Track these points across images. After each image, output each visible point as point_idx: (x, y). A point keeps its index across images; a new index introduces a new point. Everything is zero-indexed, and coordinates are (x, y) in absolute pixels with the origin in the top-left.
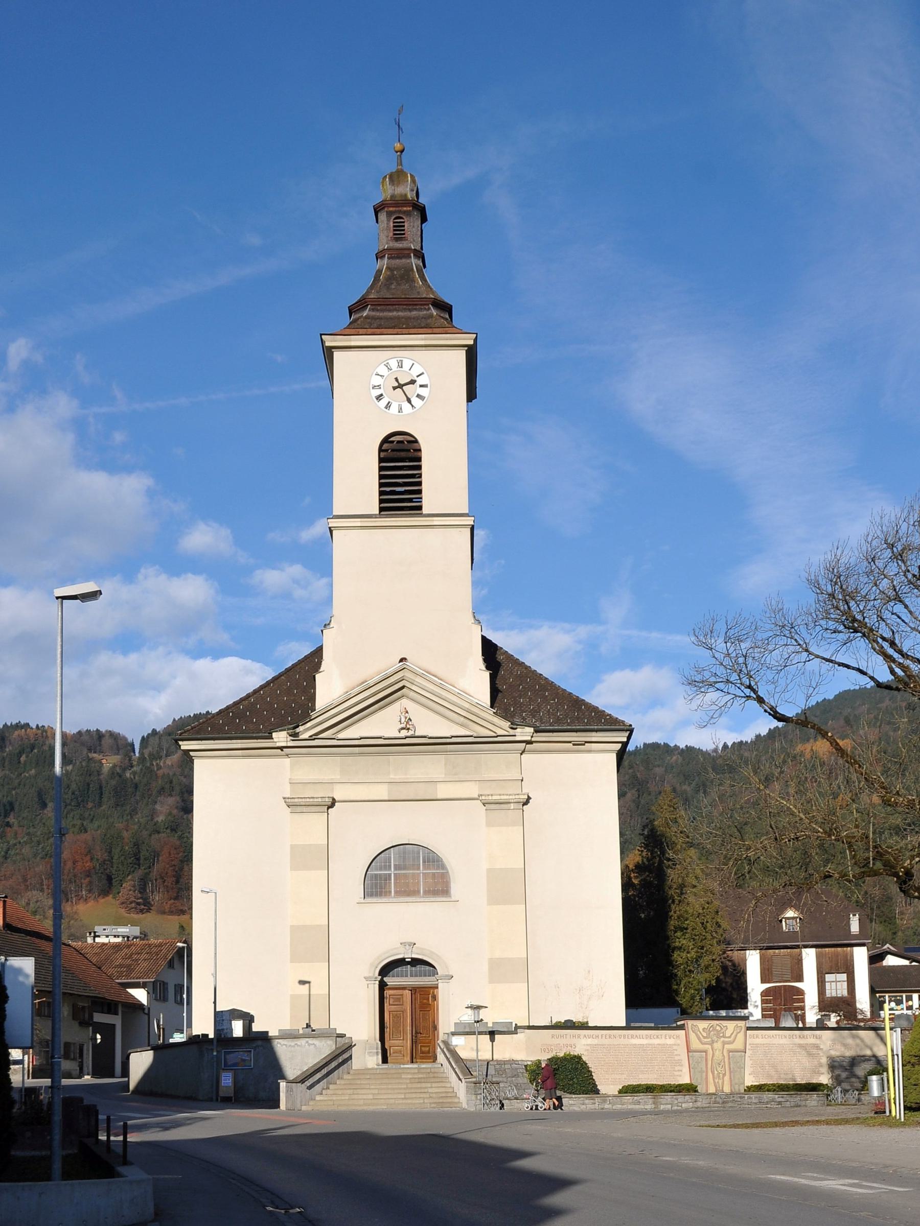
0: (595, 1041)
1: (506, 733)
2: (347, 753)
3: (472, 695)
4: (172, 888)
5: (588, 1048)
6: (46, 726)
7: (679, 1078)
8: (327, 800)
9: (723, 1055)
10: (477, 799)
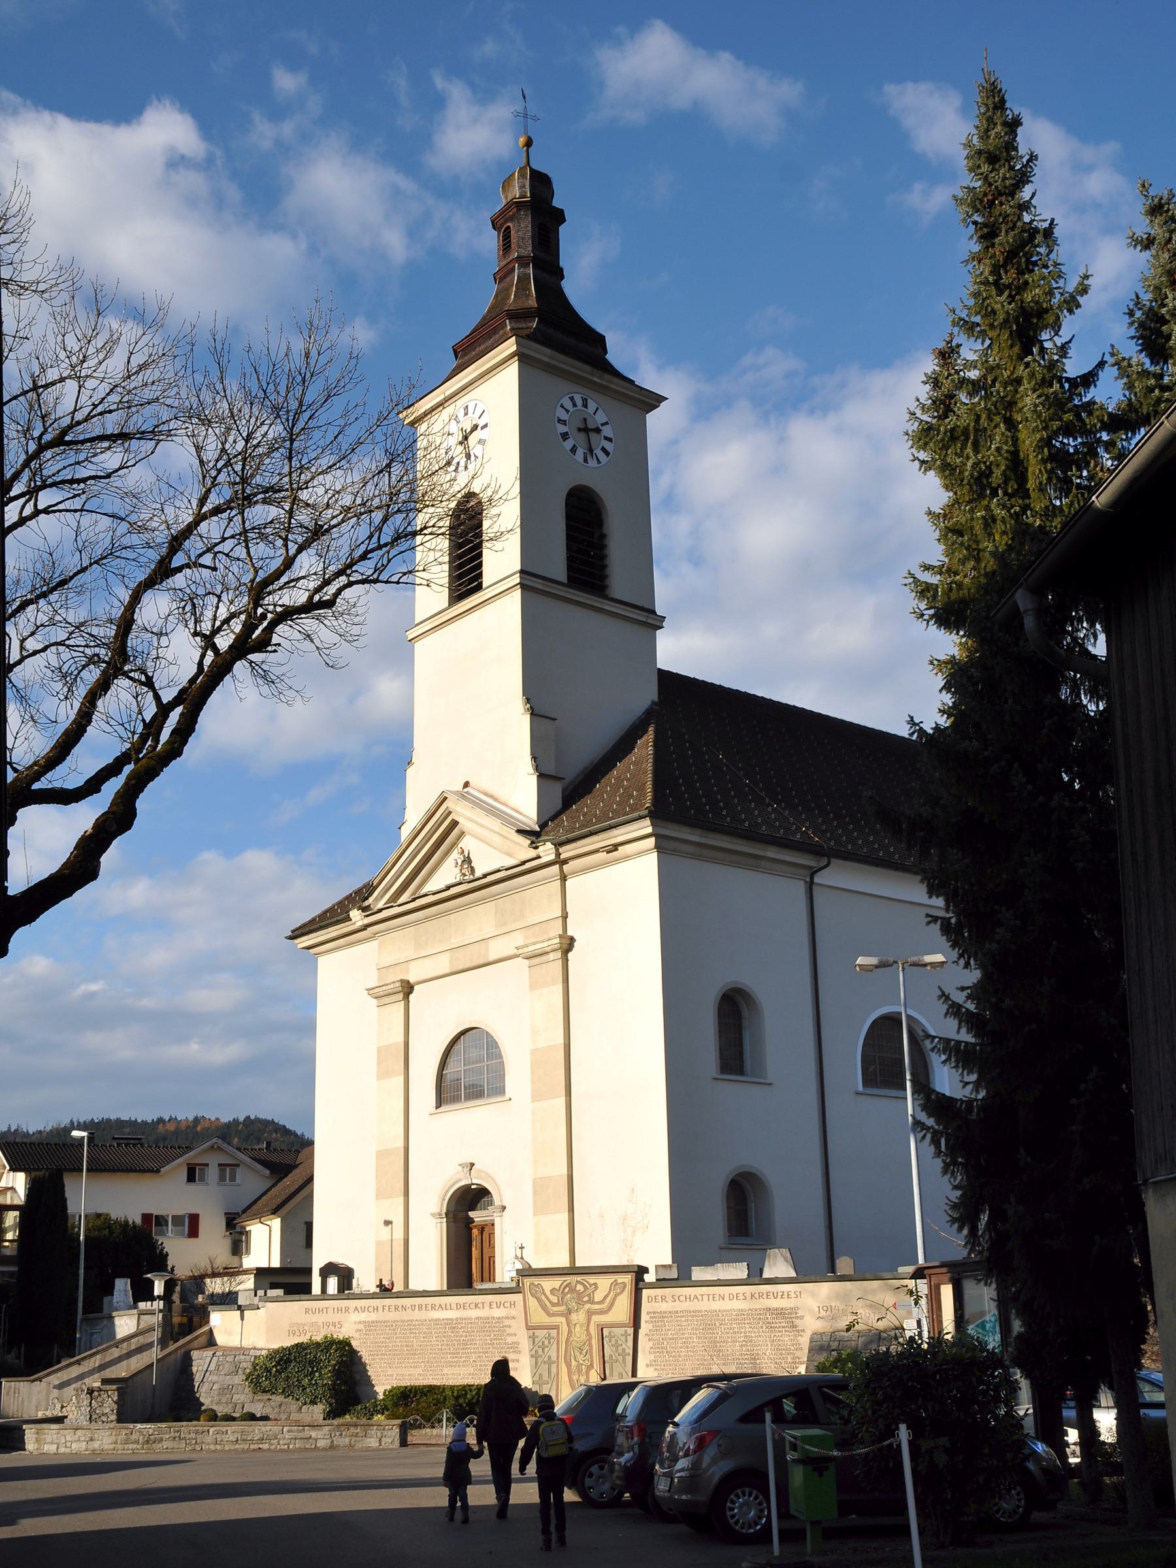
0: (373, 1317)
2: (395, 926)
5: (361, 1327)
9: (589, 1334)
10: (517, 956)
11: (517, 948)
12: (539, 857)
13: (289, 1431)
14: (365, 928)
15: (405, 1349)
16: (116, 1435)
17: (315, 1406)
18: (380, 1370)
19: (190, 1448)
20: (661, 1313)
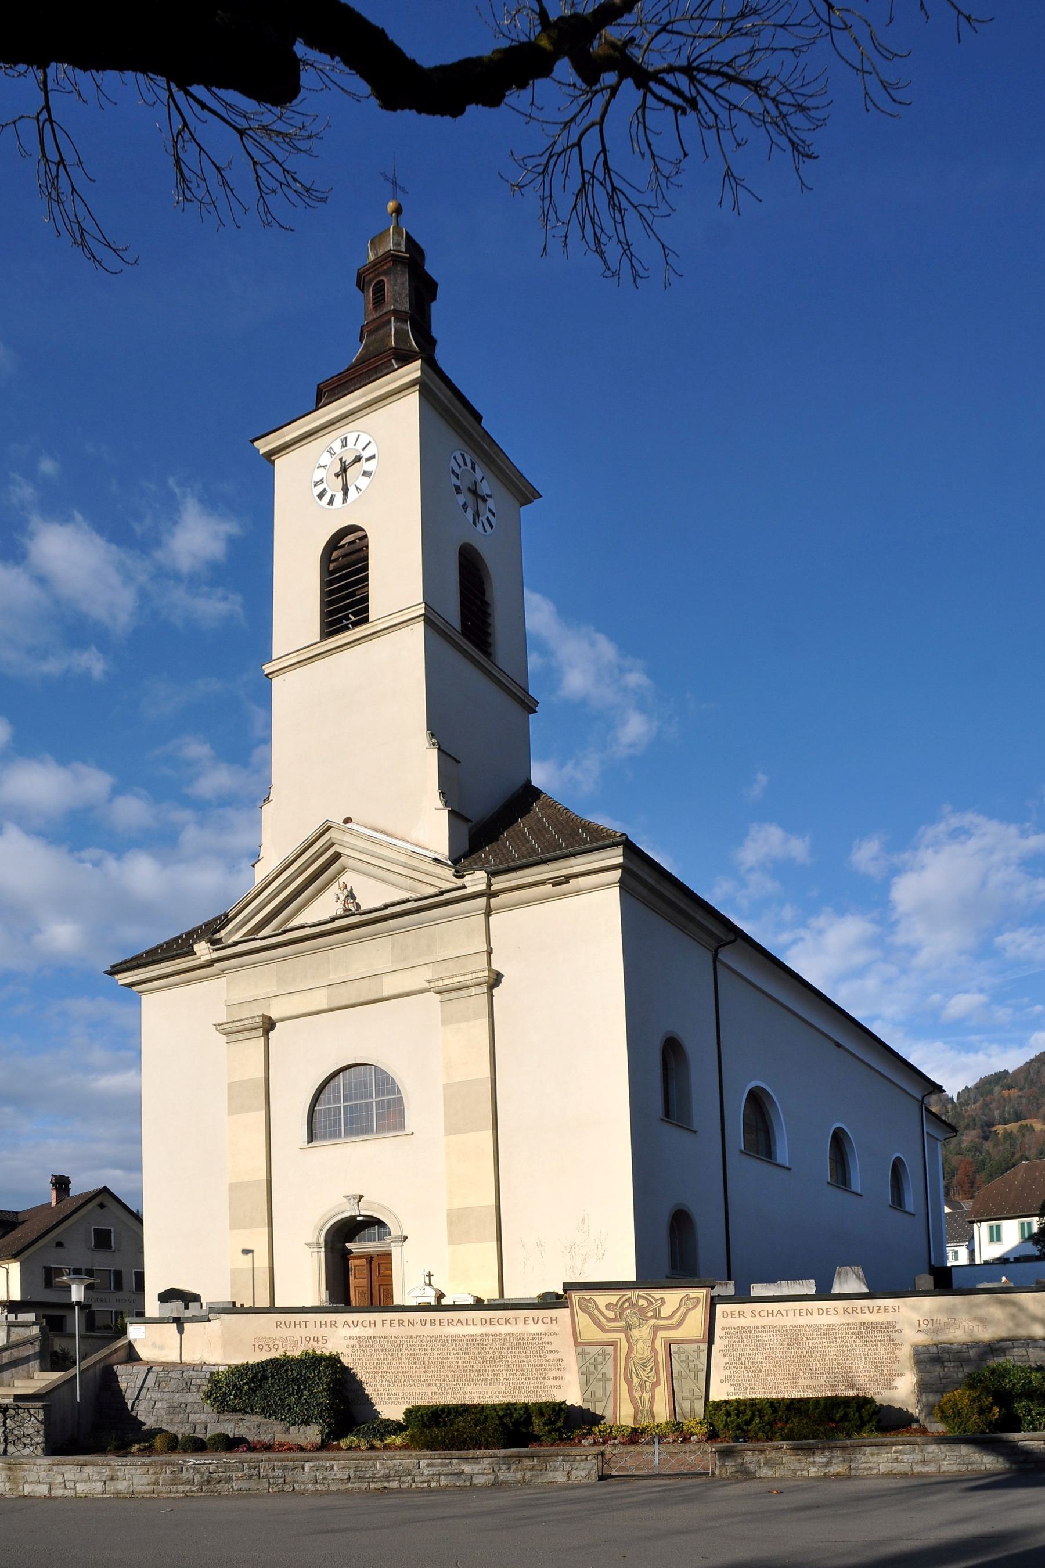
0: (370, 1332)
1: (452, 886)
2: (279, 956)
3: (426, 846)
4: (968, 1191)
5: (354, 1342)
7: (554, 1391)
8: (257, 1020)
11: (428, 982)
12: (464, 887)
13: (428, 1466)
14: (211, 963)
15: (414, 1366)
16: (156, 1473)
17: (309, 1427)
18: (381, 1389)
19: (276, 1489)
20: (738, 1328)
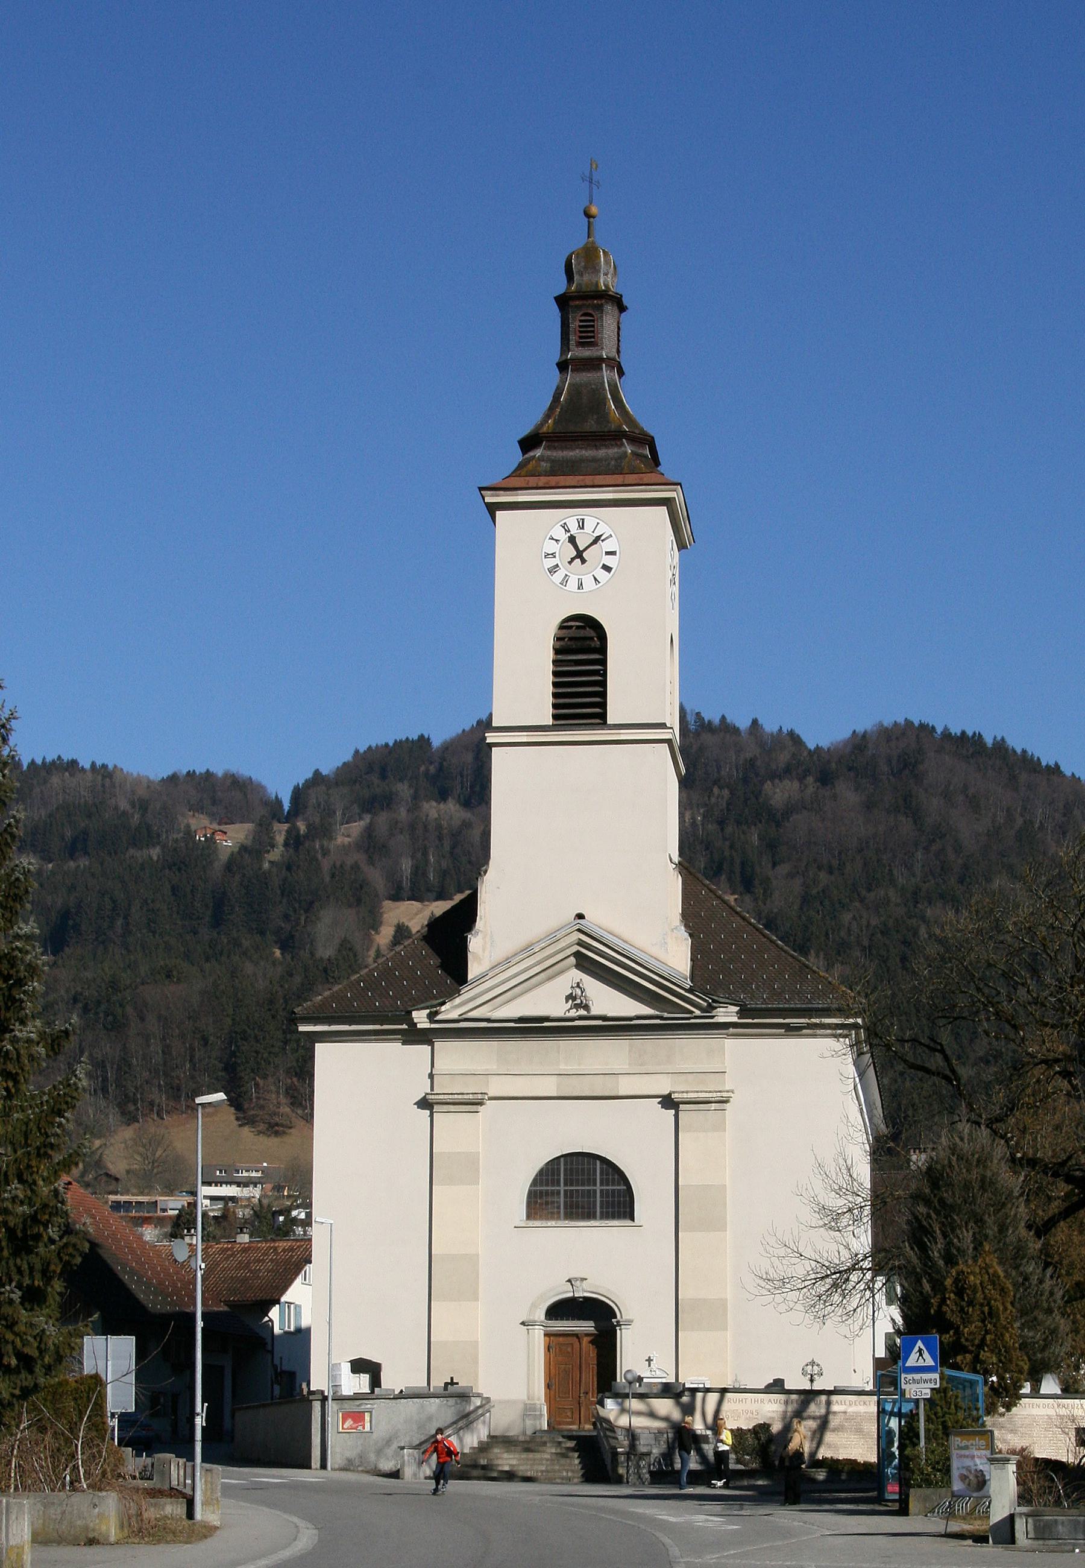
6: (111, 767)
